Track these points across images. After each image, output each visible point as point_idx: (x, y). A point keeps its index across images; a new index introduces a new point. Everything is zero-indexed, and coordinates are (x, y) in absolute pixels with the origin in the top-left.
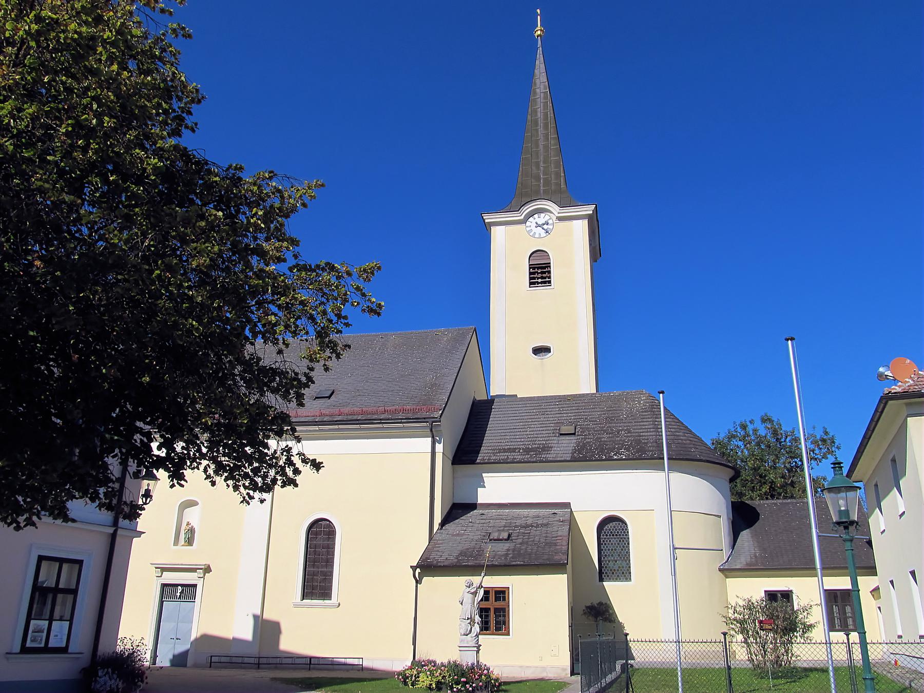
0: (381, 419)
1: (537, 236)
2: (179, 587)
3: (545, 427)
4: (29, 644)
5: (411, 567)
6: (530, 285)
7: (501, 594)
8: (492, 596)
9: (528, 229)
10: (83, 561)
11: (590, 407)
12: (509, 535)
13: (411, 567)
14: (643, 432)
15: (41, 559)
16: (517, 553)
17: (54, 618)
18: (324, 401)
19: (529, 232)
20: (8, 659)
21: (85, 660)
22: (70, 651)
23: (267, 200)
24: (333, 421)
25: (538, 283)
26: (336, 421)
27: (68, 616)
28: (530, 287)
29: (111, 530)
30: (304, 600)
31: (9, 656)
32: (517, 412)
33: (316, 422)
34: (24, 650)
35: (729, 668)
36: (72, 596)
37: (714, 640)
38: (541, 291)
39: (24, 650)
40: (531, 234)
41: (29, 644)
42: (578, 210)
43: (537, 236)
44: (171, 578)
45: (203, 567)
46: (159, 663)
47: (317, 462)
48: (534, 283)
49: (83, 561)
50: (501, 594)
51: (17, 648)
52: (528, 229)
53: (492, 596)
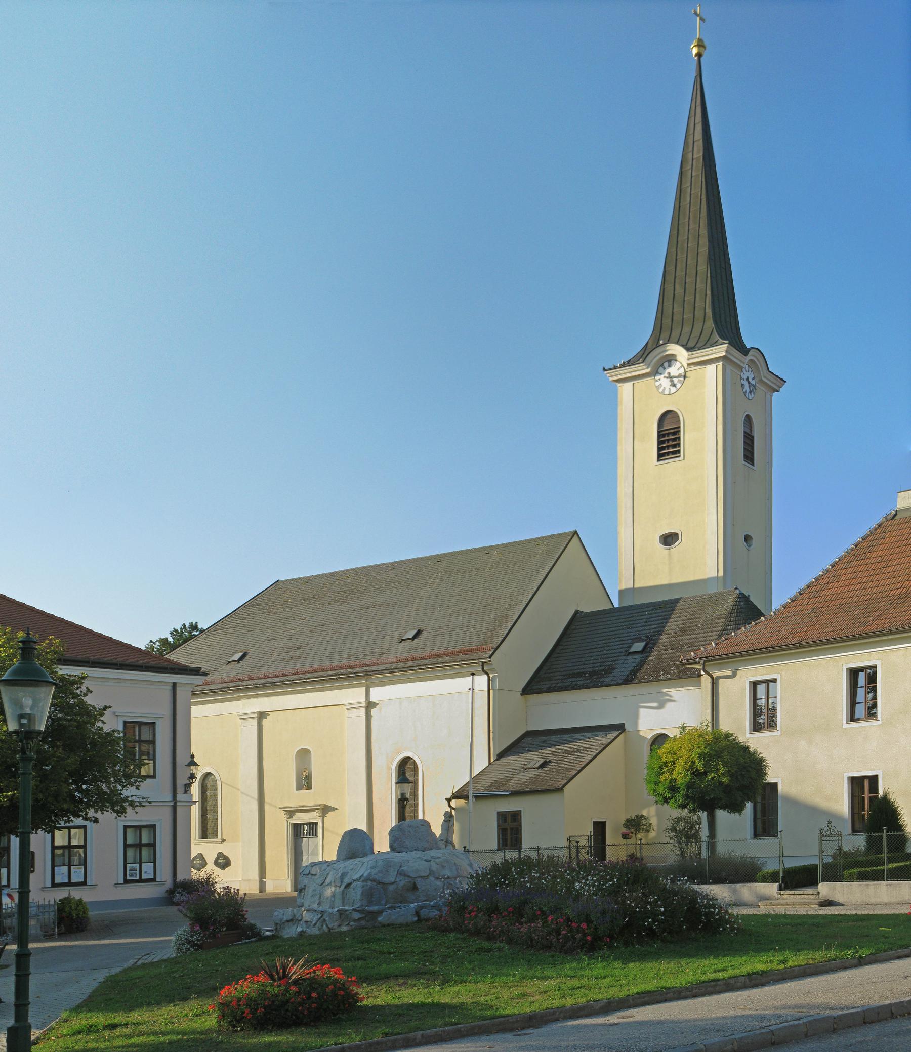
1: (667, 392)
2: (305, 826)
4: (128, 878)
5: (446, 799)
7: (516, 816)
8: (509, 819)
9: (657, 383)
13: (446, 799)
17: (56, 865)
18: (406, 644)
19: (658, 387)
20: (116, 887)
21: (169, 884)
22: (157, 880)
23: (58, 747)
24: (405, 668)
25: (668, 454)
26: (408, 667)
27: (152, 860)
29: (172, 803)
31: (117, 885)
32: (607, 627)
34: (126, 881)
35: (69, 867)
36: (153, 848)
37: (725, 840)
38: (670, 464)
39: (126, 881)
40: (661, 390)
41: (128, 878)
42: (704, 354)
44: (299, 818)
45: (319, 807)
46: (270, 888)
47: (50, 834)
48: (663, 455)
50: (516, 816)
51: (121, 881)
52: (657, 383)
53: (509, 819)
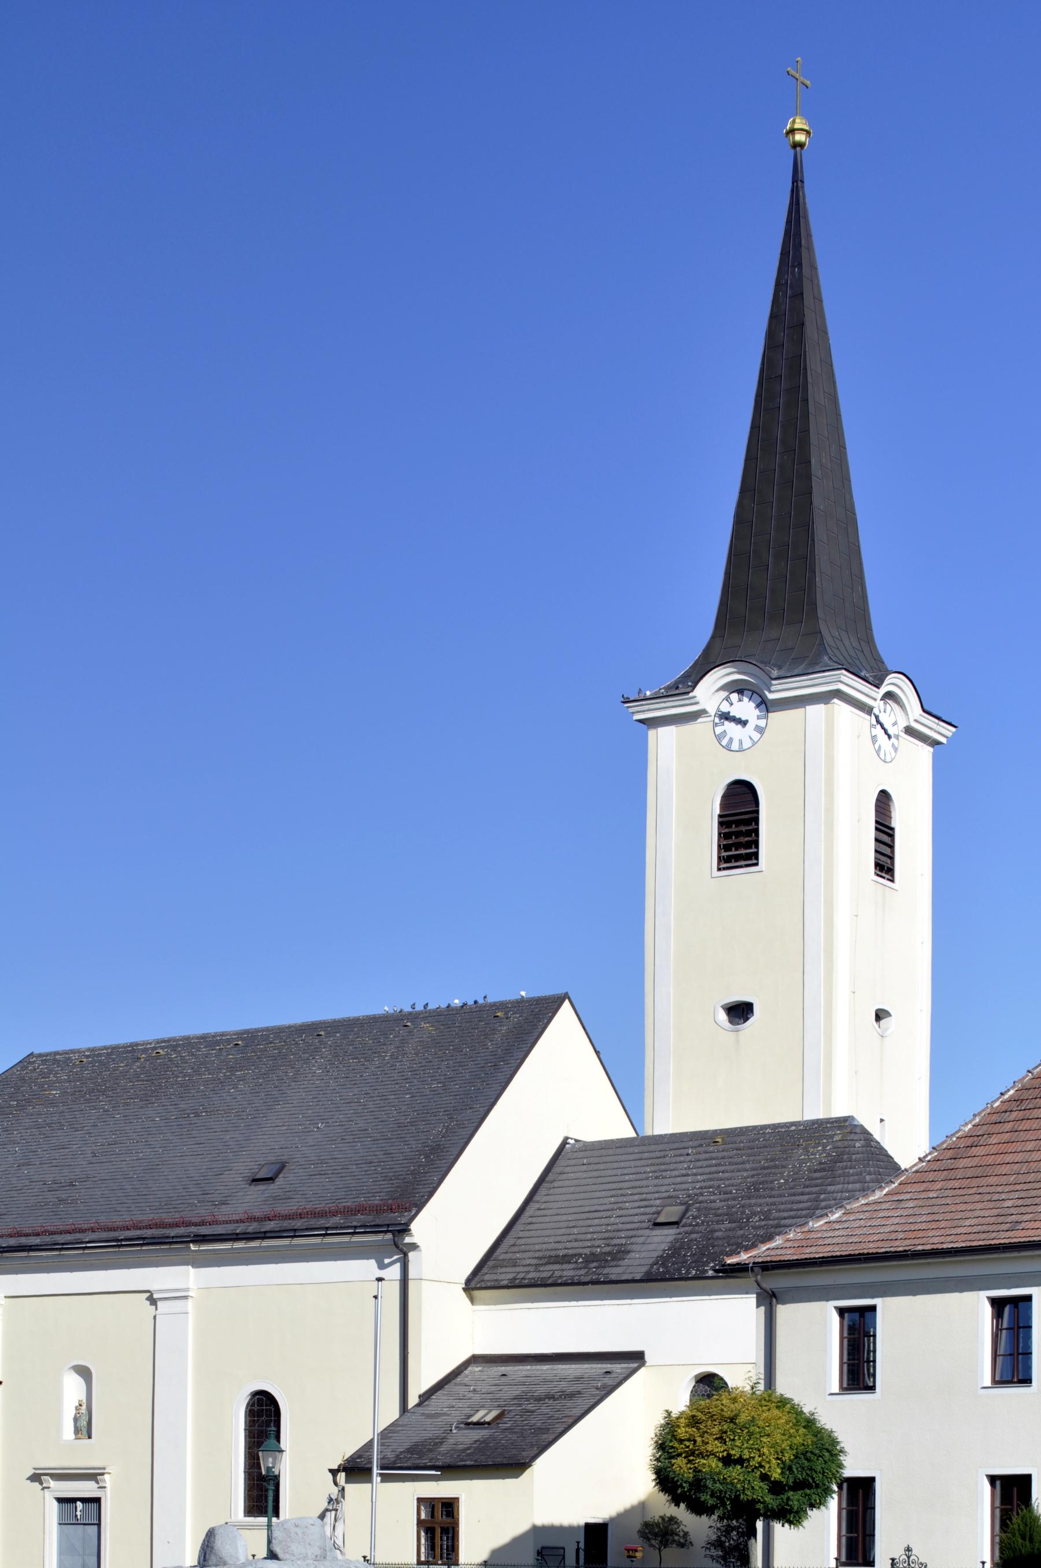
0: (327, 1229)
1: (747, 744)
3: (646, 1207)
5: (331, 1471)
6: (719, 864)
7: (449, 1507)
10: (872, 1480)
11: (740, 1159)
12: (770, 1388)
13: (331, 1471)
14: (785, 1218)
15: (564, 1549)
16: (482, 1446)
28: (719, 869)
30: (55, 1503)
33: (237, 1234)
38: (740, 877)
40: (724, 742)
43: (735, 746)
49: (872, 1480)
